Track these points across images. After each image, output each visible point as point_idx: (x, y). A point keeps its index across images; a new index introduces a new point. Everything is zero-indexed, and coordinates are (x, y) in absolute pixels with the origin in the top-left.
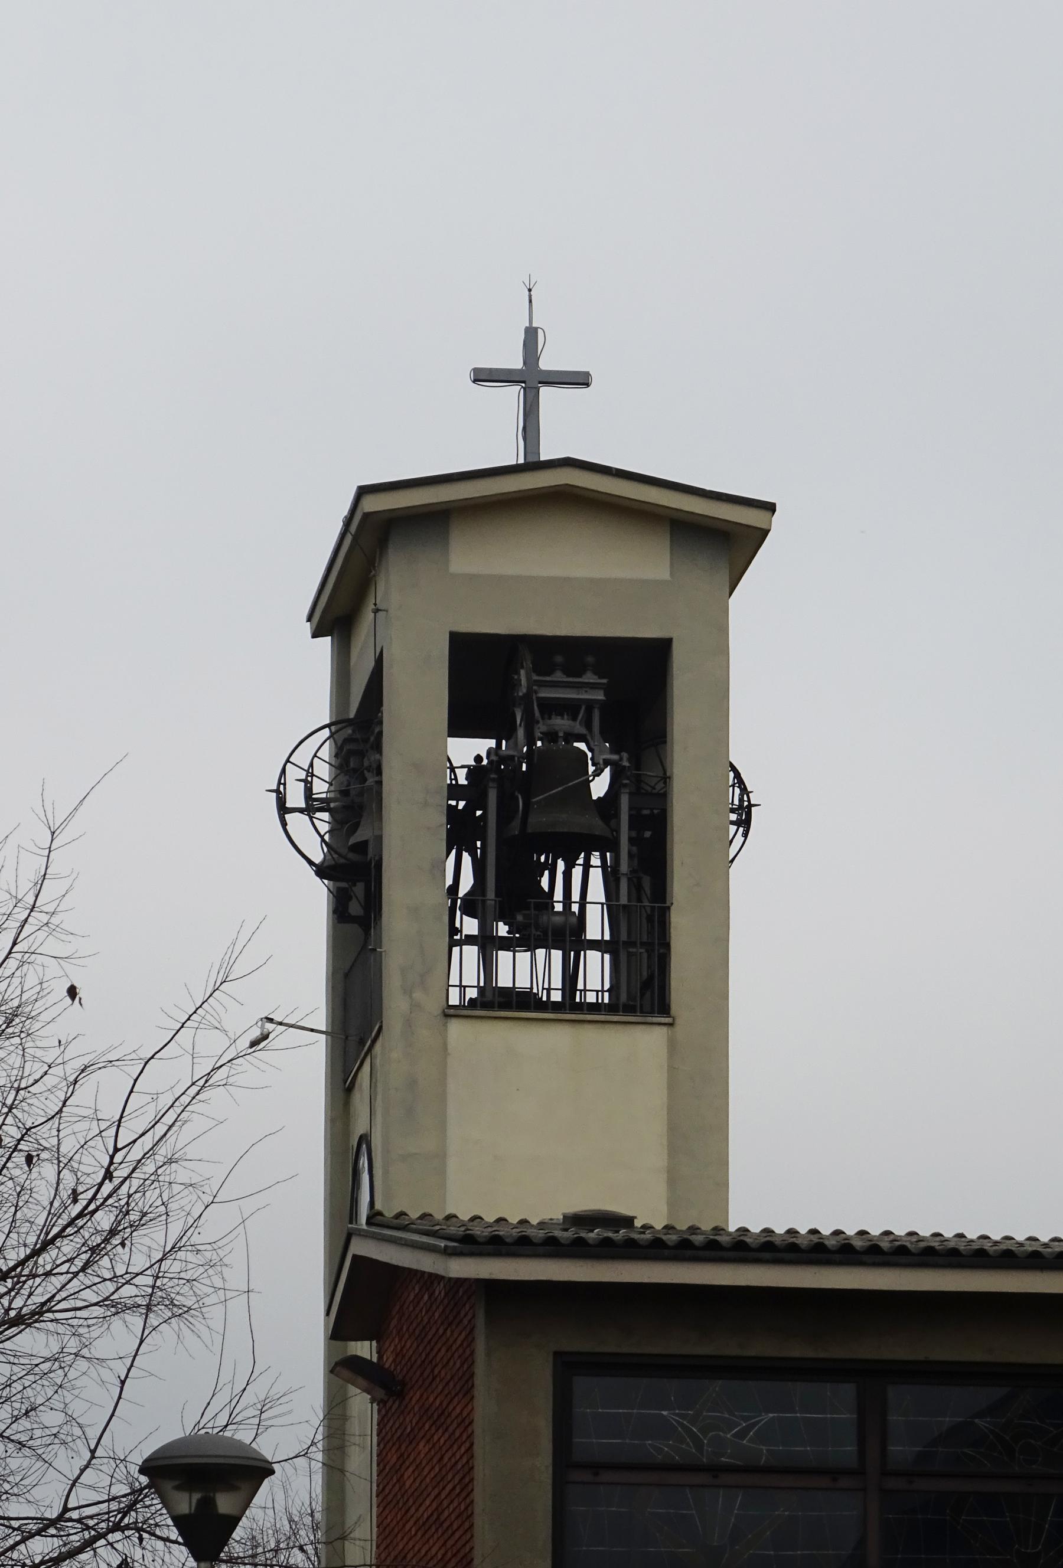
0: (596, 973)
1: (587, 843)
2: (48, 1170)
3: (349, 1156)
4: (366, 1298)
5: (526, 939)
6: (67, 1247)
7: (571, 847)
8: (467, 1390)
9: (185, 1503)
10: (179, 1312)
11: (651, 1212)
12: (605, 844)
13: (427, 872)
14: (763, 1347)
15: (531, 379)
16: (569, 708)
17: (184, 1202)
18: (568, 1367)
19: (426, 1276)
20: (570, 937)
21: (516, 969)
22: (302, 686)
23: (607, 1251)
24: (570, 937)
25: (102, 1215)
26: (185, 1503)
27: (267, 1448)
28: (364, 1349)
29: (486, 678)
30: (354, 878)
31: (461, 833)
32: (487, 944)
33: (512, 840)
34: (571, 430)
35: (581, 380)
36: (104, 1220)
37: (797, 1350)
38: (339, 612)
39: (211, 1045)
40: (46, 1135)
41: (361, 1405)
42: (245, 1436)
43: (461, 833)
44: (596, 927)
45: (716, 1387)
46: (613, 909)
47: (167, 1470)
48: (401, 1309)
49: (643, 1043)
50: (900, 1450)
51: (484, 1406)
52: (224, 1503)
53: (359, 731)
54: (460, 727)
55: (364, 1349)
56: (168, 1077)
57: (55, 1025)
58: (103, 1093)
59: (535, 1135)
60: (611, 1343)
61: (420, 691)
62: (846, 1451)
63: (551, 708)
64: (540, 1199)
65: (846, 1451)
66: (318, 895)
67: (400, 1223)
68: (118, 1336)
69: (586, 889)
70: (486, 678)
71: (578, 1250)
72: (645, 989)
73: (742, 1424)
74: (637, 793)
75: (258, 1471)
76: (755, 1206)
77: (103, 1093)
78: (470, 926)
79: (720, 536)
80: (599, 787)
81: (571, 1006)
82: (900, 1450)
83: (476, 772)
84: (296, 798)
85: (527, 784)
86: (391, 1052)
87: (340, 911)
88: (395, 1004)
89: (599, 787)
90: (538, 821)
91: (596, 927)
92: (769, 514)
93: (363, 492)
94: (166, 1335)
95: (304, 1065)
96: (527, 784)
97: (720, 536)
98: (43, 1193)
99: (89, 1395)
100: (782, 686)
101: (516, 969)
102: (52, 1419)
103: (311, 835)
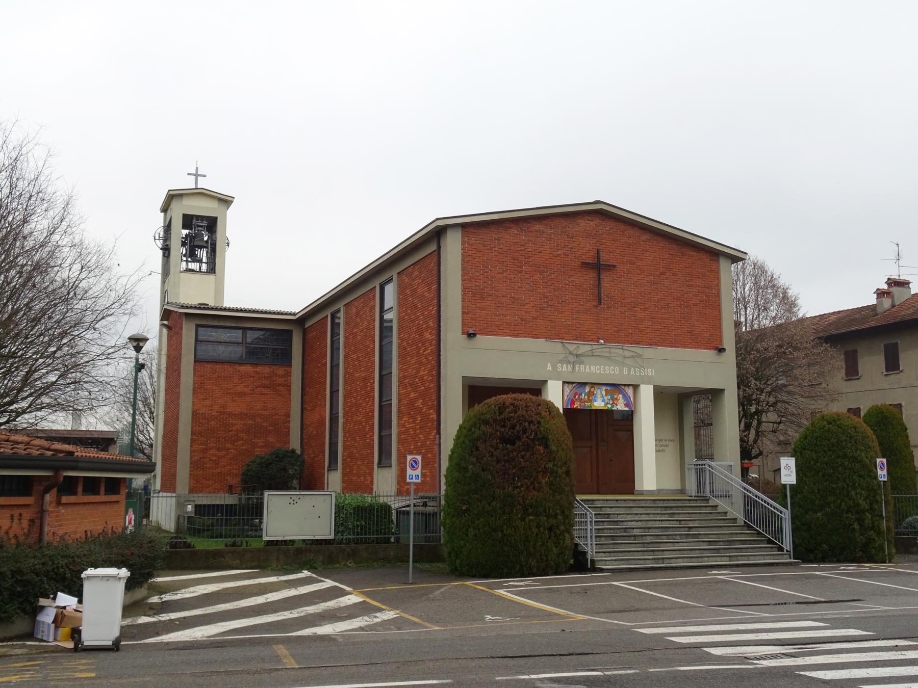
0: (204, 267)
1: (204, 247)
2: (114, 292)
3: (164, 293)
4: (166, 315)
5: (193, 261)
6: (117, 304)
7: (201, 247)
8: (181, 329)
9: (135, 344)
10: (135, 315)
11: (212, 304)
12: (207, 247)
13: (178, 250)
14: (222, 324)
15: (197, 175)
16: (201, 226)
17: (136, 298)
18: (198, 326)
19: (659, 448)
20: (200, 261)
21: (192, 266)
22: (159, 220)
23: (204, 309)
24: (200, 261)
25: (122, 300)
26: (135, 344)
27: (148, 337)
28: (166, 322)
29: (188, 221)
30: (166, 250)
31: (183, 244)
32: (187, 261)
33: (192, 247)
34: (203, 184)
35: (205, 176)
36: (123, 300)
37: (233, 325)
38: (165, 210)
39: (141, 274)
40: (114, 287)
41: (165, 331)
42: (145, 334)
43: (183, 244)
44: (205, 260)
45: (221, 330)
46: (207, 258)
47: (131, 339)
48: (171, 318)
49: (211, 278)
50: (249, 340)
51: (184, 331)
52: (141, 344)
53: (168, 228)
54: (184, 227)
55: (166, 322)
56: (134, 279)
57: (116, 270)
58: (123, 281)
59: (194, 291)
60: (204, 323)
61: (177, 222)
62: (240, 340)
63: (198, 226)
64: (195, 302)
65: (240, 340)
66: (161, 252)
67: (172, 303)
68: (126, 318)
69: (203, 254)
70: (188, 221)
71: (200, 308)
72: (212, 270)
73: (224, 335)
74: (212, 240)
75: (147, 340)
76: (227, 304)
77: (123, 281)
78: (184, 259)
79: (226, 201)
80: (206, 239)
81: (200, 271)
82: (249, 340)
83: (186, 235)
84: (157, 237)
85: (194, 238)
86: (171, 277)
87: (164, 255)
88: (172, 270)
89: (206, 239)
90: (196, 243)
91: (205, 260)
92: (201, 354)
93: (172, 197)
94: (132, 319)
95: (158, 278)
96: (194, 238)
97: (226, 201)
98: (113, 296)
99: (120, 327)
100: (233, 226)
101: (192, 266)
102: (113, 331)
103: (160, 243)
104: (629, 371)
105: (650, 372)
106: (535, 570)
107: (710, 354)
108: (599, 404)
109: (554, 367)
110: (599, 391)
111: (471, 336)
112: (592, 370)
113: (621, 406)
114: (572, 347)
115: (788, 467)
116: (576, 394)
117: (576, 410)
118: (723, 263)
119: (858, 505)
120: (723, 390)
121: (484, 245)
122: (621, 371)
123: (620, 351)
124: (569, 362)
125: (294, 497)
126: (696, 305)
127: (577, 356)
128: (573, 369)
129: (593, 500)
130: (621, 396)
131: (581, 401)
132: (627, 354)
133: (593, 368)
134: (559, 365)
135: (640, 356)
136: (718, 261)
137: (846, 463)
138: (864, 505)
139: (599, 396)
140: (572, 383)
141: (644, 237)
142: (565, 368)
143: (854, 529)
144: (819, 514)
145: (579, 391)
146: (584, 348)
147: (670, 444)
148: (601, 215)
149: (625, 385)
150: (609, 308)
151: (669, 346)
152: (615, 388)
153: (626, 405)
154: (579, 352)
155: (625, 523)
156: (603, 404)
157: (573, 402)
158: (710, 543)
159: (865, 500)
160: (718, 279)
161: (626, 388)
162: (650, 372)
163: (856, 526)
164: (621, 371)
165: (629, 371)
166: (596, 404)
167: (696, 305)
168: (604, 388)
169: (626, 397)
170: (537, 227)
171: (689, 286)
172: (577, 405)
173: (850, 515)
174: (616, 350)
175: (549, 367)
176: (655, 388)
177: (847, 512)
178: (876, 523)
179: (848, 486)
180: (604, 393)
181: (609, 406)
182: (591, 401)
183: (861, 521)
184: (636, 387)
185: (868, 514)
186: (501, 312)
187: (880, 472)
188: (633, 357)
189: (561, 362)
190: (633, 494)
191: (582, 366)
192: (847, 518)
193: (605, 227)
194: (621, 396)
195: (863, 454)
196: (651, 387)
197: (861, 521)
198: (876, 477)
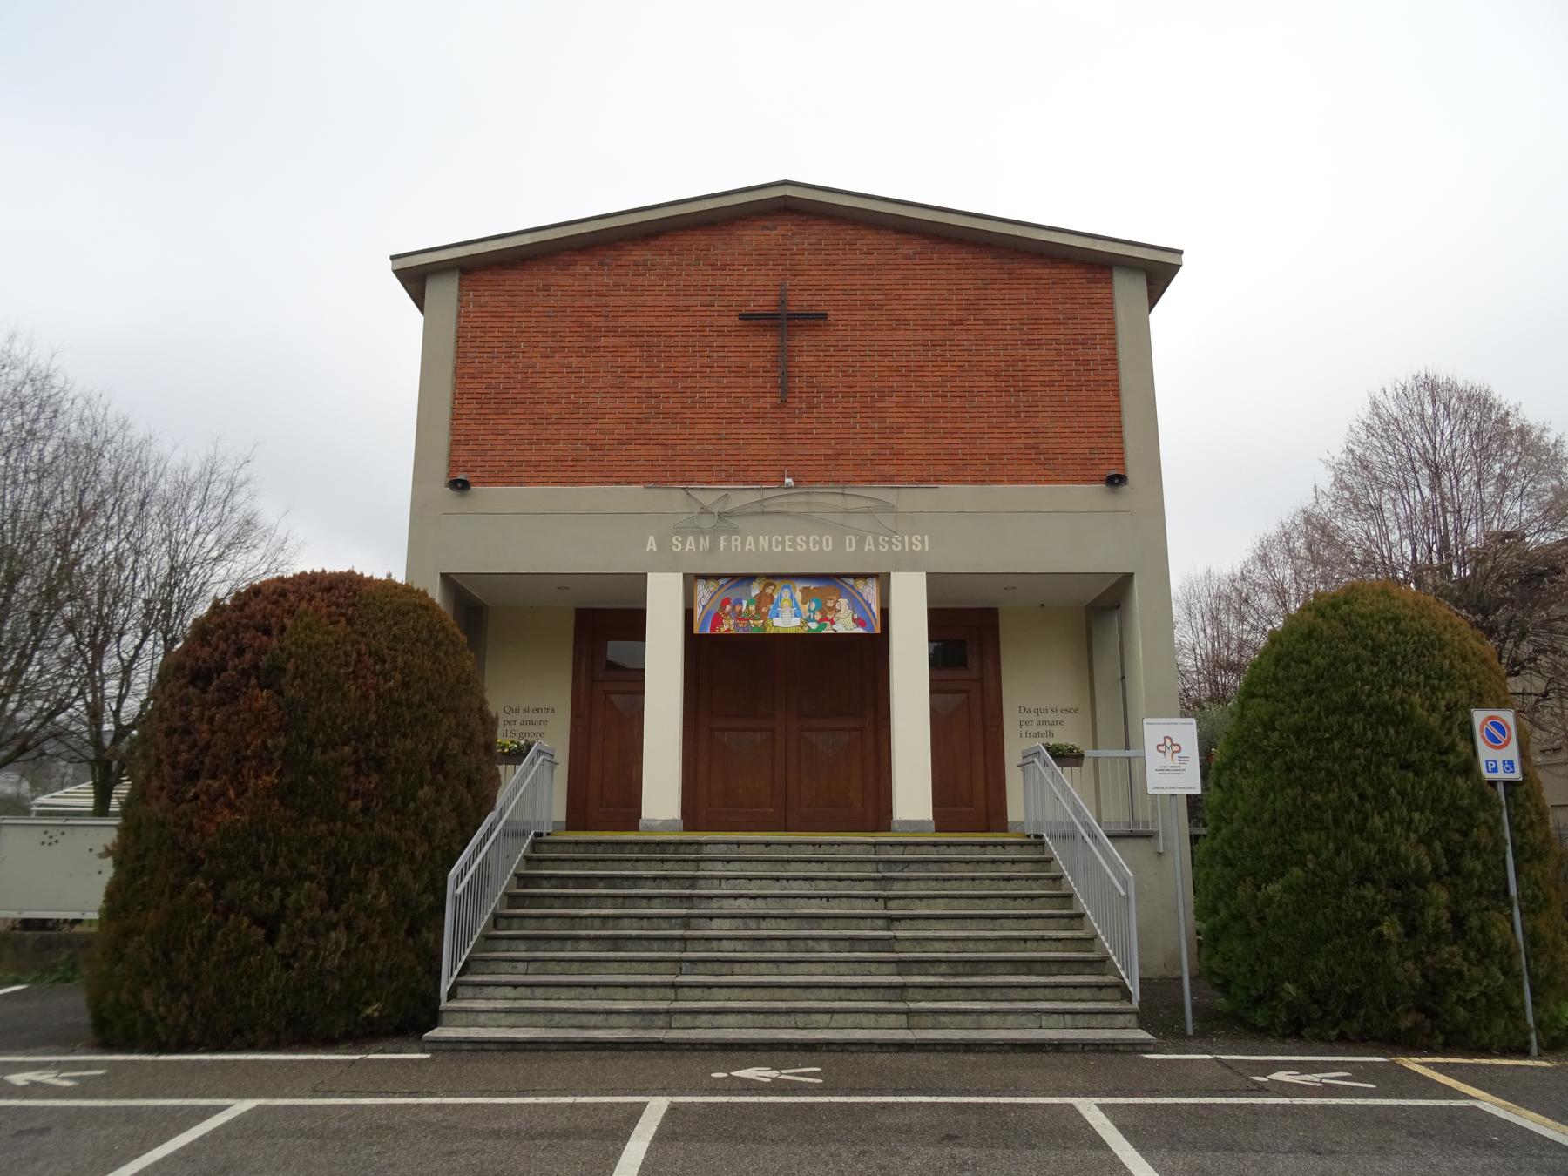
104: (861, 542)
105: (919, 543)
106: (194, 1035)
107: (1093, 493)
108: (786, 621)
109: (664, 544)
110: (786, 594)
111: (459, 486)
112: (758, 545)
113: (844, 624)
114: (707, 498)
115: (1169, 746)
116: (726, 602)
117: (727, 637)
118: (1127, 289)
119: (1396, 856)
120: (1132, 575)
121: (511, 303)
122: (839, 544)
123: (838, 501)
124: (699, 532)
125: (52, 831)
126: (1050, 384)
127: (722, 516)
128: (714, 544)
129: (699, 843)
130: (844, 602)
131: (739, 616)
132: (853, 504)
133: (764, 542)
134: (676, 540)
135: (889, 509)
136: (1110, 281)
137: (1357, 728)
138: (1418, 856)
139: (786, 602)
140: (717, 577)
141: (908, 249)
142: (690, 547)
143: (1381, 942)
144: (1274, 888)
145: (733, 594)
146: (741, 498)
147: (1066, 717)
148: (788, 210)
149: (855, 576)
150: (811, 407)
151: (975, 482)
152: (831, 581)
153: (860, 622)
154: (730, 507)
155: (715, 903)
156: (796, 622)
157: (717, 620)
158: (903, 966)
159: (1425, 840)
160: (1112, 321)
161: (860, 585)
162: (919, 543)
163: (1390, 928)
164: (839, 544)
165: (861, 542)
166: (777, 622)
167: (1050, 384)
168: (800, 585)
169: (857, 603)
170: (639, 254)
171: (1030, 343)
172: (728, 626)
173: (1369, 892)
174: (827, 500)
175: (651, 544)
176: (934, 580)
177: (1361, 882)
178: (1474, 921)
179: (1362, 796)
180: (799, 596)
181: (814, 626)
182: (764, 616)
183: (1409, 912)
184: (884, 580)
185: (1434, 888)
186: (545, 435)
187: (1485, 752)
188: (868, 511)
189: (682, 530)
190: (1005, 830)
191: (736, 541)
192: (1359, 900)
193: (803, 239)
194: (844, 602)
195: (1416, 699)
196: (920, 580)
197: (1409, 912)
198: (1469, 766)
